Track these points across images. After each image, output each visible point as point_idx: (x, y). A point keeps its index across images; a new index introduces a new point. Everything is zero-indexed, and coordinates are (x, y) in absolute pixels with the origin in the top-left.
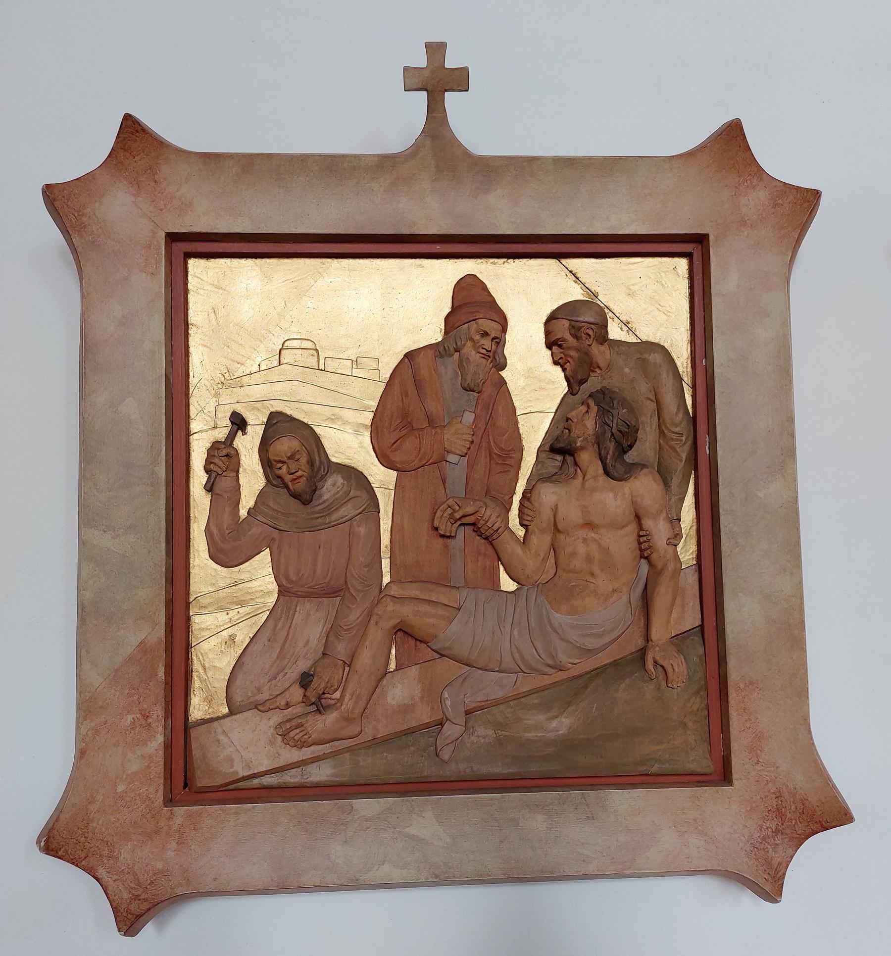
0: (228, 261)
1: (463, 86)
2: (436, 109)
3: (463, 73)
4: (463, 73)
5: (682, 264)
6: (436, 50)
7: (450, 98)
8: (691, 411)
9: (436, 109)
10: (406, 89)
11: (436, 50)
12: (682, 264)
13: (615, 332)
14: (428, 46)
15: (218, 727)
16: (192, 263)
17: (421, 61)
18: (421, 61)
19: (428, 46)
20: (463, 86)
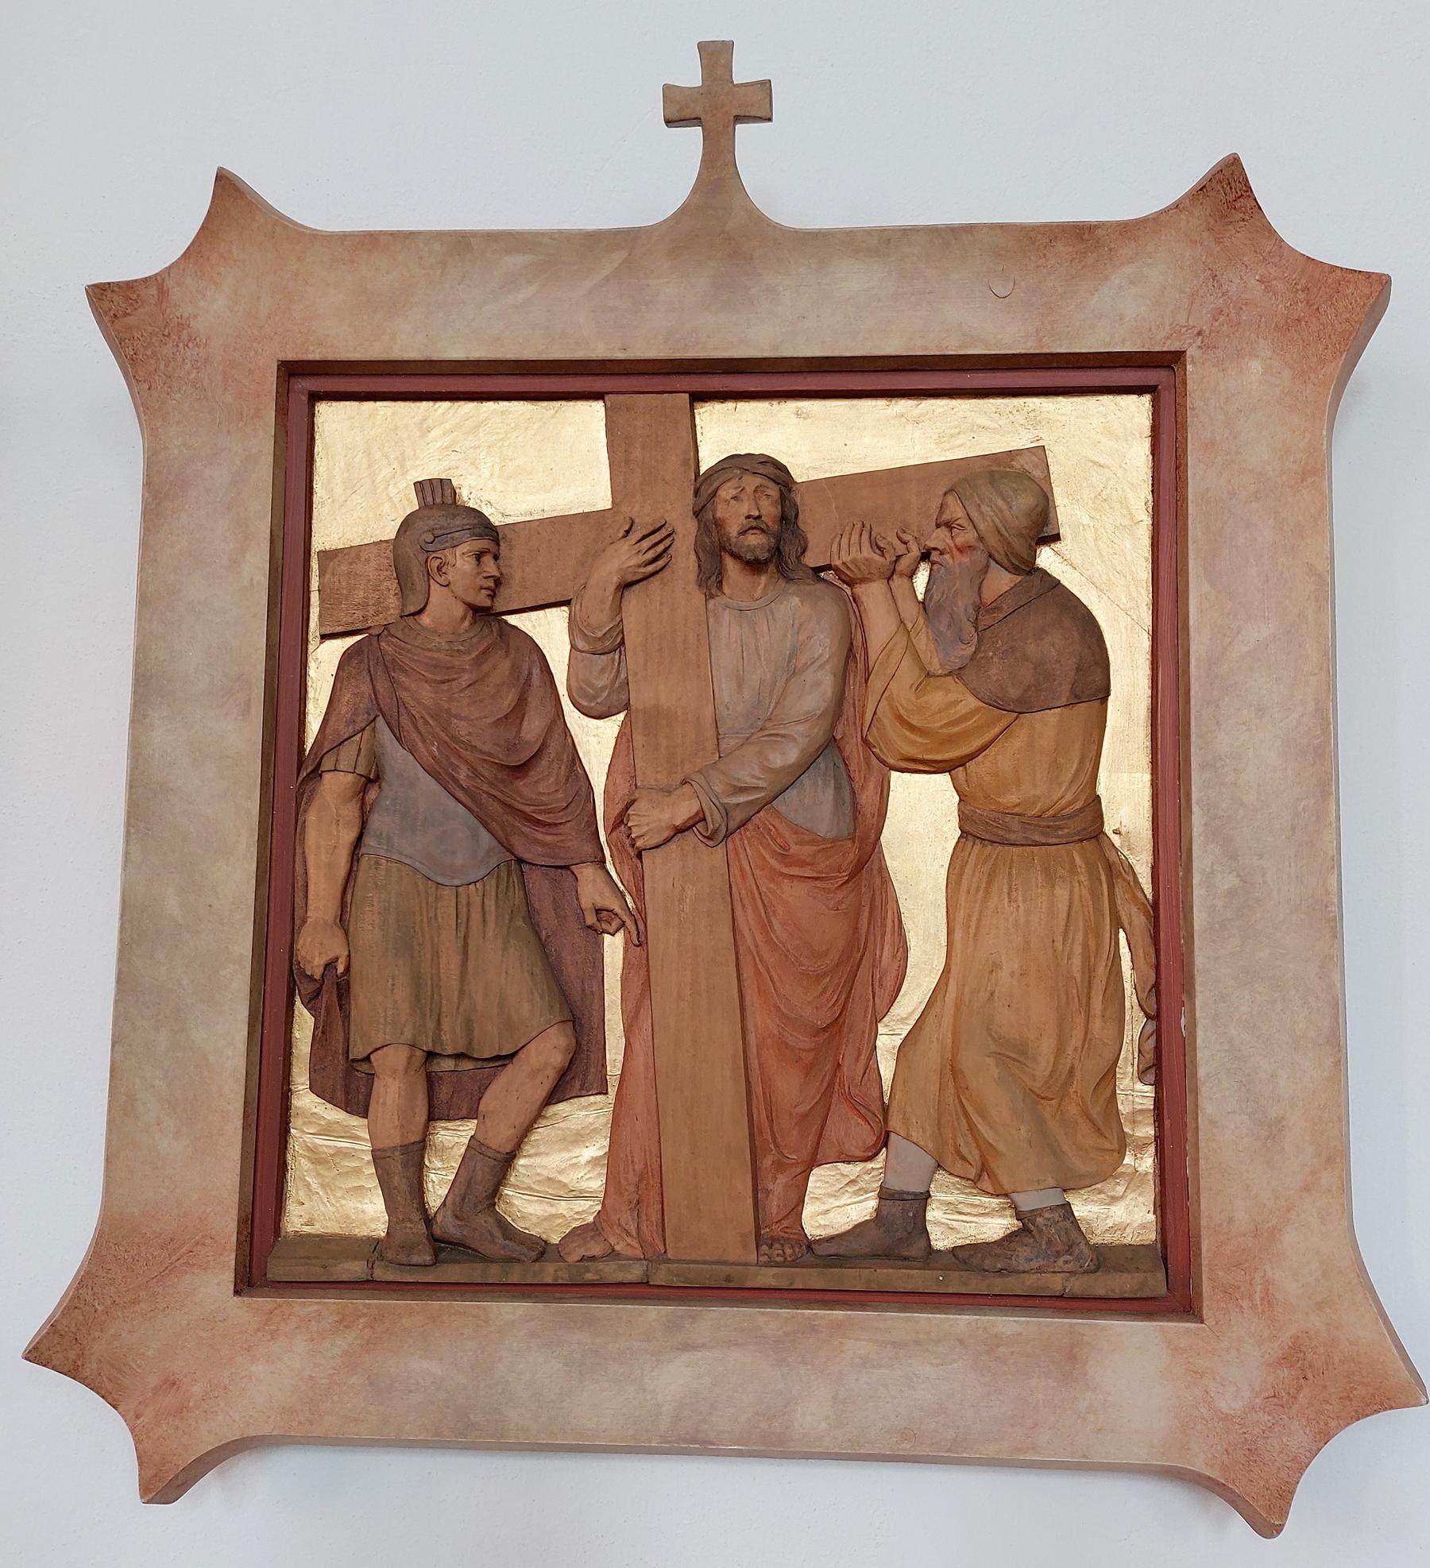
1: (670, 93)
6: (716, 55)
17: (691, 76)
18: (691, 76)
20: (670, 93)
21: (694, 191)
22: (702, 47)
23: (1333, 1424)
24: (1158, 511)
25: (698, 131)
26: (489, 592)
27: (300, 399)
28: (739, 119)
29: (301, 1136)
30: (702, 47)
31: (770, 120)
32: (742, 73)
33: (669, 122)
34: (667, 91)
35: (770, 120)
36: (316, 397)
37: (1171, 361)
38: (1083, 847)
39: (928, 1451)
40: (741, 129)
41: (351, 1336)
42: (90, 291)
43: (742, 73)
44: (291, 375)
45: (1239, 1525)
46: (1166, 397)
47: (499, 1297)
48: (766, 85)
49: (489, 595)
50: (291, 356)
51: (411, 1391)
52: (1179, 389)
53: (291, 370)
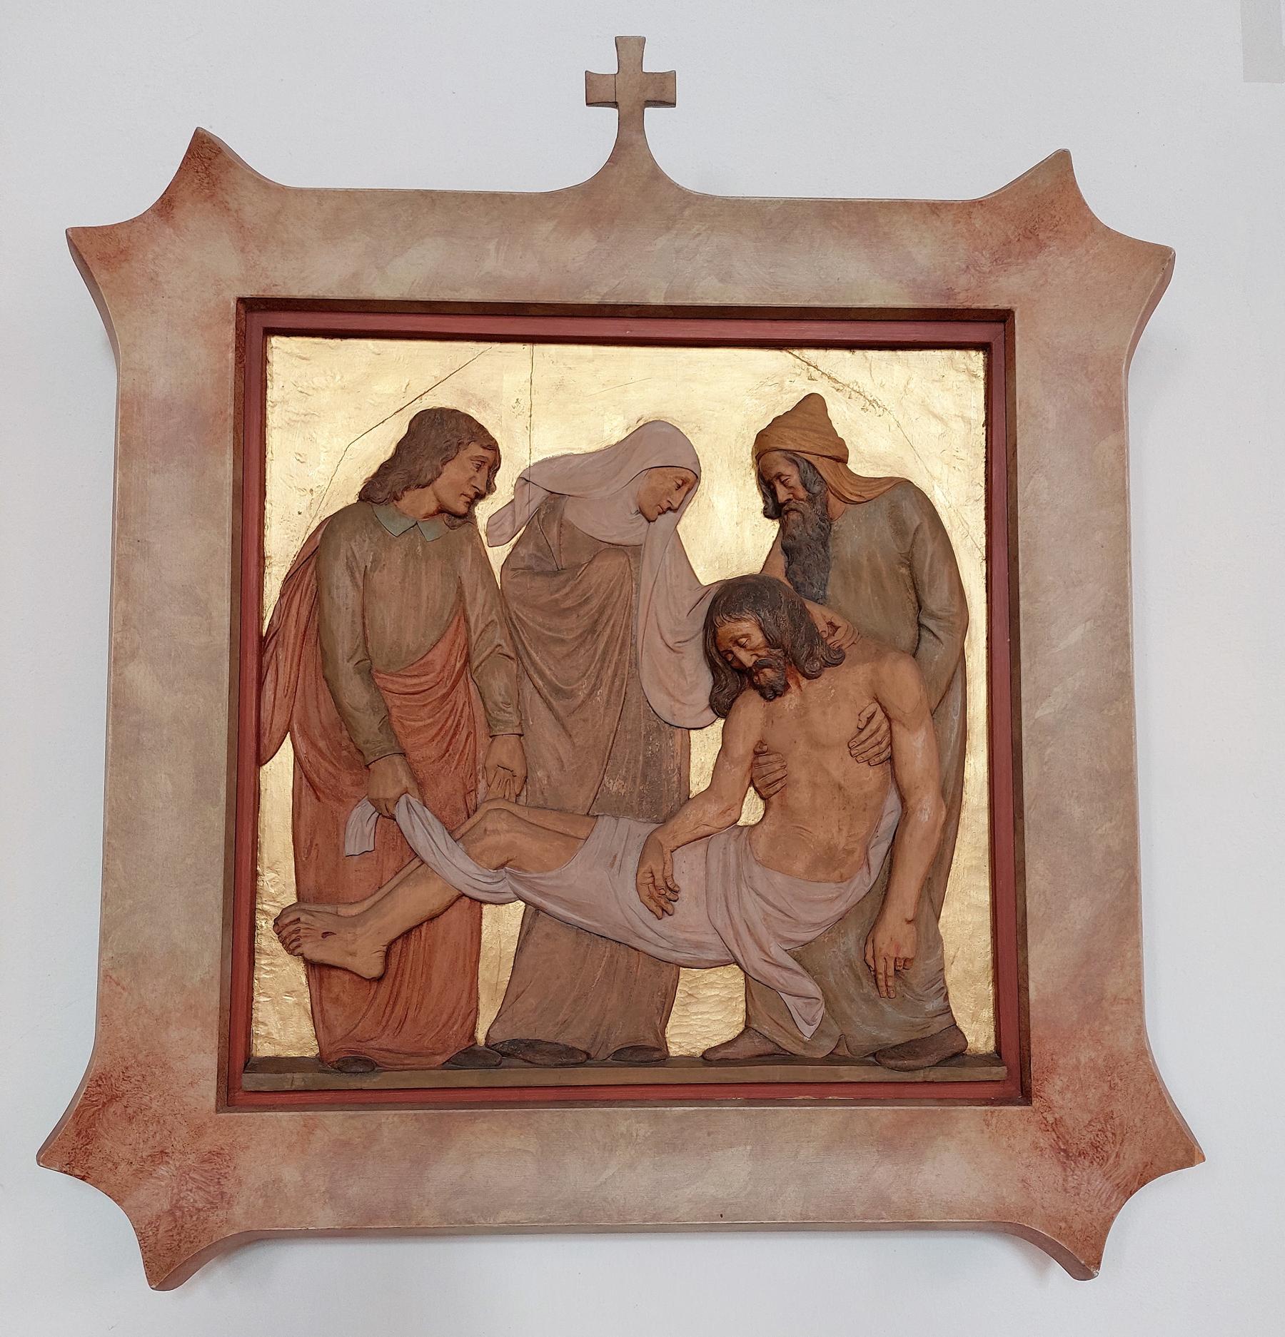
0: (370, 343)
1: (591, 80)
2: (631, 127)
3: (668, 79)
4: (668, 79)
5: (976, 360)
6: (630, 48)
7: (652, 115)
8: (499, 585)
9: (631, 127)
10: (589, 102)
11: (630, 48)
12: (976, 360)
13: (855, 465)
14: (620, 42)
15: (1109, 996)
16: (275, 341)
17: (607, 65)
18: (607, 65)
19: (620, 42)
20: (591, 80)
21: (1143, 1052)
24: (261, 453)
25: (613, 113)
26: (469, 500)
27: (257, 334)
29: (263, 976)
31: (673, 105)
35: (673, 105)
42: (70, 233)
45: (1057, 1271)
46: (998, 349)
47: (375, 1243)
49: (467, 502)
50: (248, 293)
52: (991, 350)
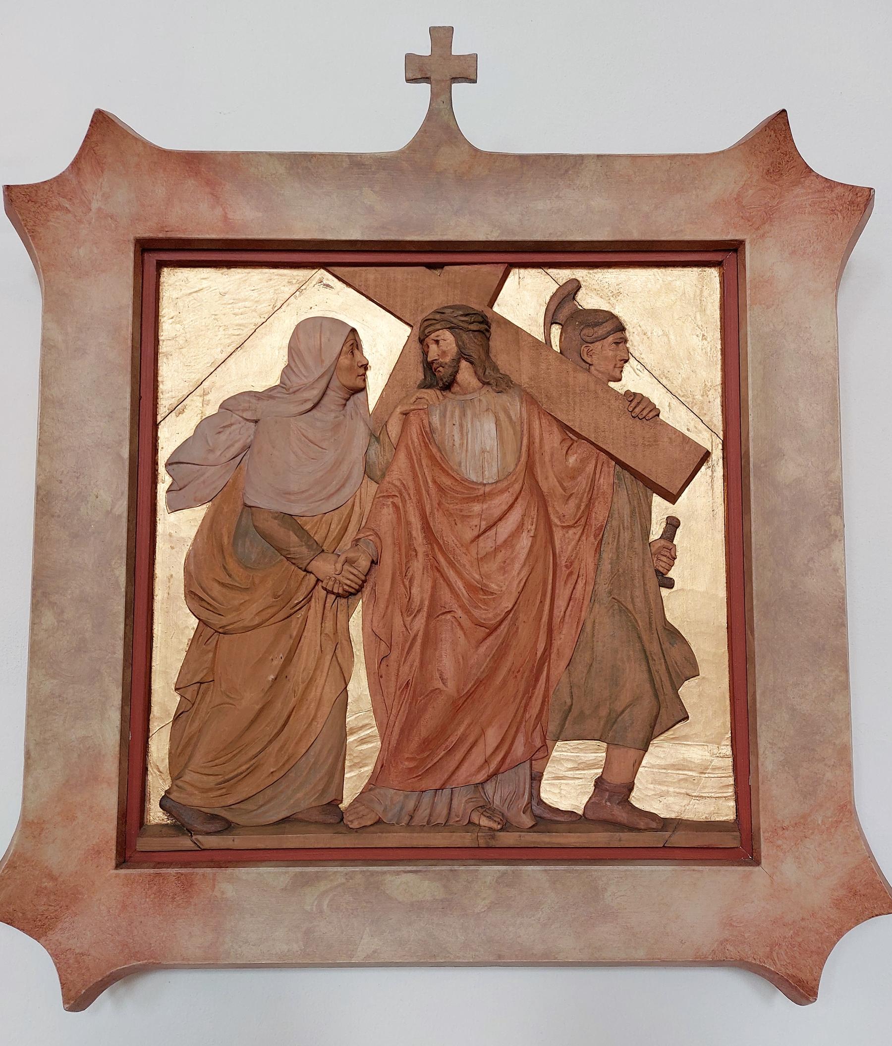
17: (424, 48)
18: (424, 48)
22: (433, 30)
23: (48, 686)
28: (455, 79)
30: (433, 30)
31: (475, 81)
32: (459, 48)
33: (408, 81)
34: (409, 58)
36: (161, 265)
37: (735, 248)
38: (729, 766)
39: (317, 961)
40: (455, 87)
41: (46, 865)
43: (459, 48)
44: (152, 259)
48: (475, 57)
51: (803, 928)
52: (740, 266)
53: (144, 247)
